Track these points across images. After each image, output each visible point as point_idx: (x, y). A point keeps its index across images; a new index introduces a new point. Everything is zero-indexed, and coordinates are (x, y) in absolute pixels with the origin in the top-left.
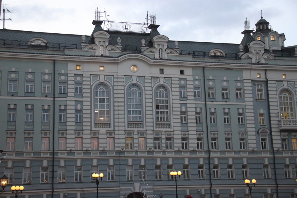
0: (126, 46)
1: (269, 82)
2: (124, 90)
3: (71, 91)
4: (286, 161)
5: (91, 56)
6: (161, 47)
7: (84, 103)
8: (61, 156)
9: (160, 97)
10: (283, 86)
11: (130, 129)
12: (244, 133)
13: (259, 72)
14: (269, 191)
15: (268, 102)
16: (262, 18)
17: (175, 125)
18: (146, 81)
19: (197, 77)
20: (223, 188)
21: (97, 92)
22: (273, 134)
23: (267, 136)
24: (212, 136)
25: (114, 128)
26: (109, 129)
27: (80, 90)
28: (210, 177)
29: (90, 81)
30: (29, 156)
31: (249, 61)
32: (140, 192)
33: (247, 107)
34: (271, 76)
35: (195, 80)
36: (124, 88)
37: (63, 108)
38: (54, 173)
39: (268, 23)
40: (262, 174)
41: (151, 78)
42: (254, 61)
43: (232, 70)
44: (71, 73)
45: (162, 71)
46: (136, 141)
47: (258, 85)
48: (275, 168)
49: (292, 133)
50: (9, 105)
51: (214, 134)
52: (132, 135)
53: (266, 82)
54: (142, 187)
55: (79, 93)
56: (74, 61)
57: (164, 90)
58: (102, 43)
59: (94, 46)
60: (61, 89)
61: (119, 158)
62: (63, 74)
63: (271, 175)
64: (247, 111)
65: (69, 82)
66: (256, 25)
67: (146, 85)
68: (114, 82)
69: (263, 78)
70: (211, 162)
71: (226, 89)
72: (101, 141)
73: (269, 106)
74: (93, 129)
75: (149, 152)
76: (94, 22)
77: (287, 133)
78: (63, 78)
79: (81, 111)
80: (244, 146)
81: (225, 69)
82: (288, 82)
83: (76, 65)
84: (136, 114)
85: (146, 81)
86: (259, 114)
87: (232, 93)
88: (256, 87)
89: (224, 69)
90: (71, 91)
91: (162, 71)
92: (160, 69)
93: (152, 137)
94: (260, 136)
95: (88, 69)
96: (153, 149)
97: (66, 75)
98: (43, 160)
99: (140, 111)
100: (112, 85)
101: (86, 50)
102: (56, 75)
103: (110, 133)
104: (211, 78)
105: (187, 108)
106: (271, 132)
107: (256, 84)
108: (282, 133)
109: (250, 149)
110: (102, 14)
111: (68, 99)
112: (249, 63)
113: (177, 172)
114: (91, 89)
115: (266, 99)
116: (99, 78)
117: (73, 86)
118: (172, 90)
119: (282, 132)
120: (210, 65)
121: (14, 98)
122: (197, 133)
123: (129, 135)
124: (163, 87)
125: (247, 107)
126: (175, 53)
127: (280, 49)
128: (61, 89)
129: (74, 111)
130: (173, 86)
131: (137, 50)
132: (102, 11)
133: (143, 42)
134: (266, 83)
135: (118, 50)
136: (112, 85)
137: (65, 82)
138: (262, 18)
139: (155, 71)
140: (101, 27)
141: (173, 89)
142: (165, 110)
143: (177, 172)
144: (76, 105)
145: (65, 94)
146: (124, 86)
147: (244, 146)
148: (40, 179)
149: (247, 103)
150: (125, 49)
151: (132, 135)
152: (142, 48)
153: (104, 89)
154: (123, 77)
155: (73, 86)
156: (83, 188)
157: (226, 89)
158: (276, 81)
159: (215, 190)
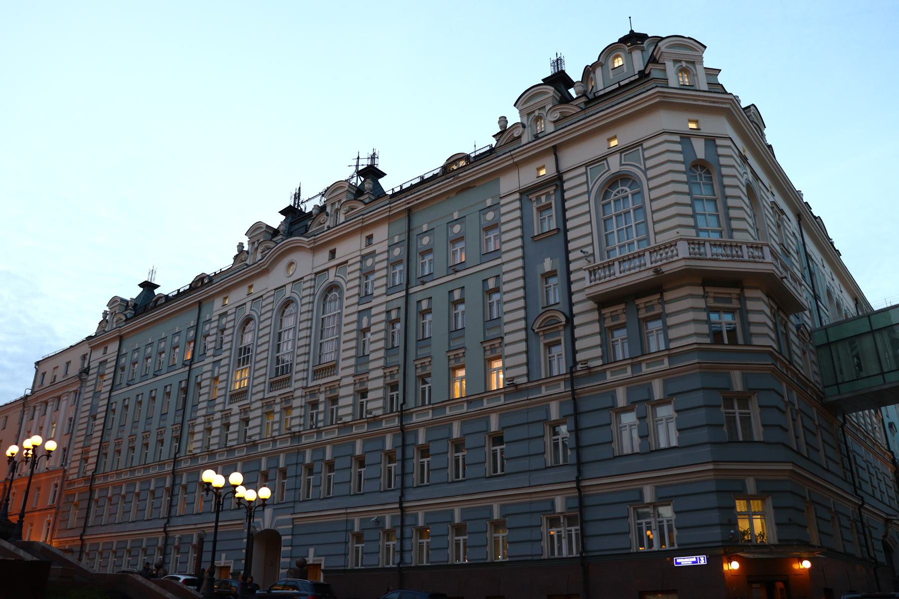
4: (284, 463)
8: (451, 413)
10: (607, 171)
14: (560, 506)
23: (562, 333)
24: (420, 372)
32: (272, 528)
35: (391, 247)
36: (314, 299)
40: (722, 426)
43: (470, 188)
49: (638, 302)
51: (423, 366)
56: (176, 311)
57: (622, 186)
61: (298, 449)
63: (761, 429)
70: (410, 440)
77: (622, 306)
81: (457, 193)
82: (621, 153)
83: (606, 141)
86: (542, 275)
89: (454, 194)
93: (302, 402)
94: (542, 338)
98: (616, 388)
99: (638, 244)
100: (643, 168)
101: (237, 266)
103: (310, 391)
106: (570, 318)
108: (708, 289)
113: (257, 492)
116: (625, 163)
118: (646, 175)
119: (708, 286)
120: (417, 200)
121: (131, 388)
122: (385, 373)
126: (358, 205)
130: (649, 164)
136: (643, 168)
143: (257, 492)
146: (314, 295)
153: (620, 188)
156: (196, 524)
158: (587, 165)
159: (416, 516)
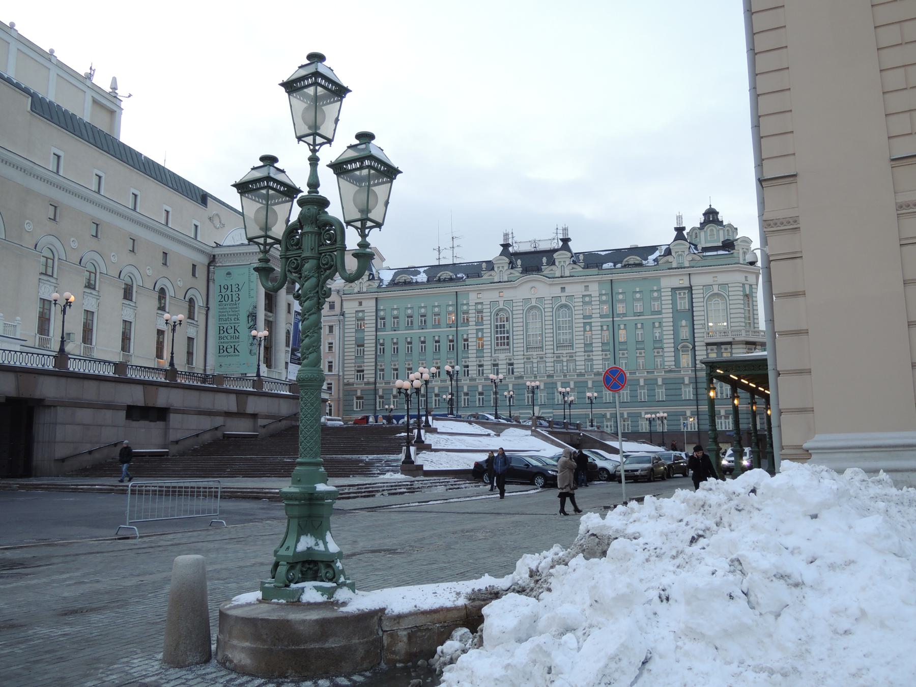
0: (526, 268)
1: (693, 288)
2: (552, 312)
3: (472, 320)
5: (491, 283)
6: (562, 264)
7: (485, 331)
9: (563, 318)
11: (528, 353)
12: (660, 350)
13: (681, 278)
15: (693, 312)
16: (710, 206)
17: (578, 346)
18: (546, 302)
19: (604, 292)
20: (679, 410)
21: (497, 319)
22: (696, 348)
25: (513, 354)
26: (541, 353)
27: (467, 320)
28: (376, 407)
29: (490, 308)
30: (381, 385)
31: (669, 266)
33: (664, 320)
34: (697, 281)
35: (601, 295)
37: (465, 337)
38: (459, 398)
39: (718, 213)
41: (702, 287)
42: (674, 265)
44: (472, 303)
45: (563, 289)
46: (535, 365)
47: (680, 293)
48: (697, 388)
50: (448, 336)
52: (532, 360)
53: (690, 288)
54: (542, 411)
55: (480, 322)
58: (501, 269)
59: (492, 273)
60: (464, 319)
62: (437, 306)
64: (664, 324)
65: (470, 312)
66: (704, 214)
67: (546, 306)
68: (513, 306)
69: (687, 284)
71: (424, 316)
72: (577, 363)
73: (693, 316)
74: (493, 355)
75: (549, 376)
76: (676, 229)
78: (465, 308)
79: (481, 339)
80: (465, 373)
84: (504, 340)
85: (546, 302)
87: (417, 320)
88: (678, 295)
90: (472, 320)
91: (563, 289)
92: (562, 288)
95: (488, 297)
96: (523, 373)
97: (467, 304)
102: (614, 294)
104: (620, 291)
105: (483, 333)
106: (694, 347)
107: (677, 292)
109: (666, 367)
110: (510, 236)
111: (469, 328)
112: (669, 269)
114: (491, 316)
115: (691, 309)
117: (474, 315)
123: (558, 359)
124: (565, 306)
125: (664, 320)
127: (721, 245)
128: (464, 319)
129: (475, 340)
130: (546, 306)
131: (538, 270)
132: (510, 233)
133: (544, 260)
134: (690, 289)
135: (517, 272)
137: (467, 313)
138: (710, 206)
139: (556, 291)
140: (568, 245)
141: (576, 308)
142: (499, 335)
144: (477, 333)
145: (466, 322)
147: (465, 373)
148: (639, 397)
149: (664, 316)
150: (526, 270)
151: (532, 360)
152: (542, 267)
154: (702, 287)
155: (474, 315)
157: (424, 316)
